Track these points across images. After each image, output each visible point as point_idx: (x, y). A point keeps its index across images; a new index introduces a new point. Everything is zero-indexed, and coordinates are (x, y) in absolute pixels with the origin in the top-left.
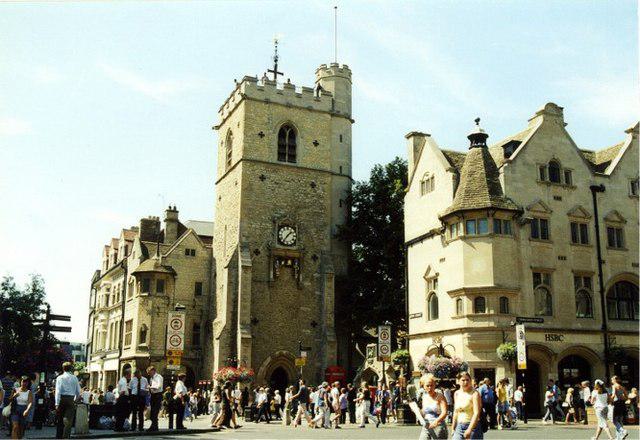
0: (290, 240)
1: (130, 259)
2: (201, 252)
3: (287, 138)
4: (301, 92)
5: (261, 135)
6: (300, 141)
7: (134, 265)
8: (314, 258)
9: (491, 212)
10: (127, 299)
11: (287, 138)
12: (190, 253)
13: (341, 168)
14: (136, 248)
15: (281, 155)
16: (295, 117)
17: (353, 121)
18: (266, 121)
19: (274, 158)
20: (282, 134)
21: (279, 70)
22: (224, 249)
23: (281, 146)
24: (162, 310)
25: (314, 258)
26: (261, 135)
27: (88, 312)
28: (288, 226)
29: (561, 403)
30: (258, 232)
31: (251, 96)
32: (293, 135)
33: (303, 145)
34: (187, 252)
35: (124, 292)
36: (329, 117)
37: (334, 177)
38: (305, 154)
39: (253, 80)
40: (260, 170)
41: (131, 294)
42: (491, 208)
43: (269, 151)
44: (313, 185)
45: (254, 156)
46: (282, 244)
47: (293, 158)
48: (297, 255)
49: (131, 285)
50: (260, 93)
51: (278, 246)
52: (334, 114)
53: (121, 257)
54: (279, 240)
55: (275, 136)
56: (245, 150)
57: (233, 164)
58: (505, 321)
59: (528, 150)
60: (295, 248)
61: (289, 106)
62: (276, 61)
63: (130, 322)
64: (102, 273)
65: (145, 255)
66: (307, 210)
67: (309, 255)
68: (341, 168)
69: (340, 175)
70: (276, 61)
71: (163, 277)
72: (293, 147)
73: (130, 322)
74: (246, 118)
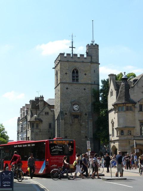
0: (76, 109)
1: (28, 116)
2: (50, 113)
3: (75, 72)
4: (79, 57)
5: (66, 74)
6: (79, 74)
7: (29, 118)
8: (86, 114)
9: (125, 104)
10: (28, 130)
11: (75, 72)
12: (47, 113)
13: (95, 82)
14: (29, 112)
15: (73, 80)
16: (78, 66)
17: (99, 64)
18: (67, 68)
19: (71, 81)
20: (73, 72)
21: (73, 47)
22: (57, 111)
23: (73, 77)
24: (38, 134)
25: (86, 114)
26: (66, 74)
27: (17, 132)
28: (76, 104)
29: (4, 160)
30: (66, 107)
31: (62, 60)
32: (77, 72)
33: (81, 76)
34: (46, 113)
35: (27, 126)
36: (90, 64)
37: (92, 85)
38: (82, 78)
39: (63, 54)
40: (67, 86)
41: (28, 128)
42: (124, 103)
43: (69, 78)
44: (85, 89)
45: (64, 81)
46: (74, 110)
47: (77, 80)
48: (80, 114)
49: (28, 125)
50: (65, 59)
51: (73, 111)
52: (91, 62)
53: (25, 115)
54: (73, 109)
55: (71, 73)
56: (61, 79)
57: (58, 84)
58: (130, 137)
59: (139, 82)
60: (78, 112)
61: (75, 62)
62: (72, 43)
63: (29, 137)
64: (20, 119)
65: (32, 116)
66: (82, 98)
67: (84, 114)
68: (95, 82)
69: (95, 84)
70: (72, 43)
71: (38, 122)
72: (77, 77)
73: (29, 137)
74: (61, 68)
